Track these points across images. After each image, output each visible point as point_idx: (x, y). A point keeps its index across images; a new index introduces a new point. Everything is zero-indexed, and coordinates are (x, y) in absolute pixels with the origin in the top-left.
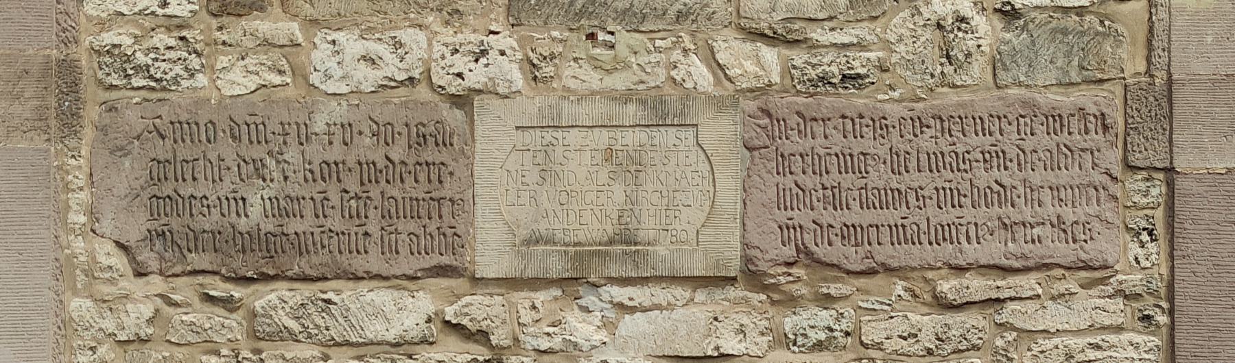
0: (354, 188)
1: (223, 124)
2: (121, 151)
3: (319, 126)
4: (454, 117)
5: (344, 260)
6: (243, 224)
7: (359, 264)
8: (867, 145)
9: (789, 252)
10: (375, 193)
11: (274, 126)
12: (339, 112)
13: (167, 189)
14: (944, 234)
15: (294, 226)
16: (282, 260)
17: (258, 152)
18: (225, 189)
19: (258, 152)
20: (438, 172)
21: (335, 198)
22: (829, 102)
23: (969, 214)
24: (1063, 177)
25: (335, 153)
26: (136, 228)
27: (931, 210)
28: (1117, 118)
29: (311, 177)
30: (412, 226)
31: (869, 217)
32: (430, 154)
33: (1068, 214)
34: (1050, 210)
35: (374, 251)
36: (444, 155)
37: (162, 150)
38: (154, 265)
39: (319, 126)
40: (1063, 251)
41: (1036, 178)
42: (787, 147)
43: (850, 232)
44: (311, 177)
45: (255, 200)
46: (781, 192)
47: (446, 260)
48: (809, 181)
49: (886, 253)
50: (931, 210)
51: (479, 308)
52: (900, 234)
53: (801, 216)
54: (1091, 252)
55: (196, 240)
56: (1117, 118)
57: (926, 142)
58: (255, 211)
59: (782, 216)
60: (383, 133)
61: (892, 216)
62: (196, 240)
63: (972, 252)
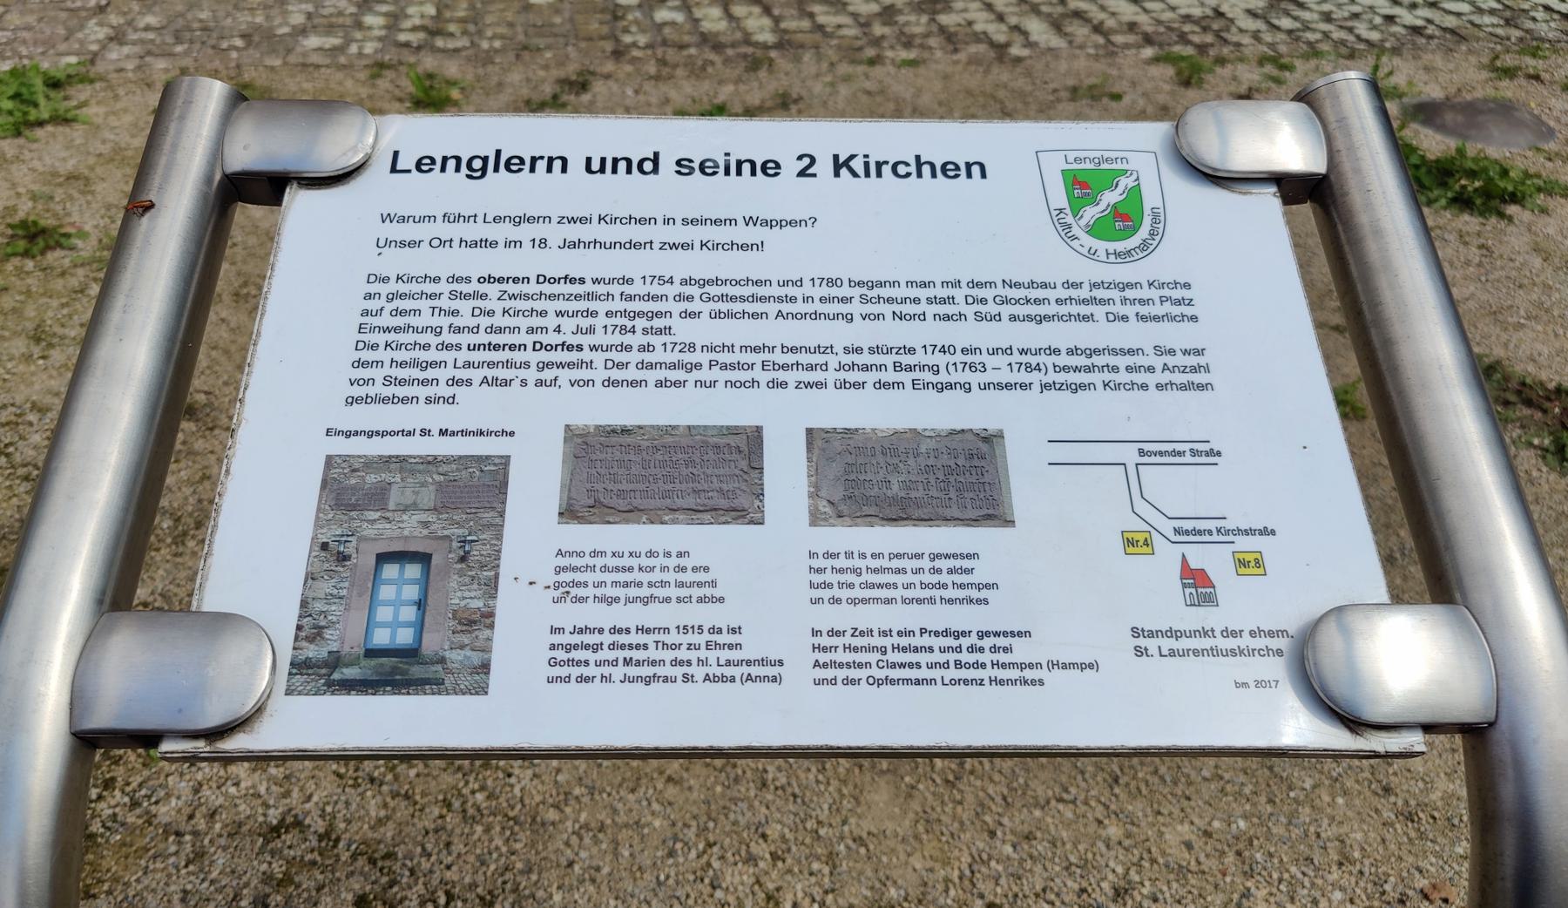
0: (942, 477)
1: (878, 449)
2: (830, 459)
3: (923, 450)
4: (984, 447)
5: (940, 511)
6: (889, 493)
7: (948, 513)
8: (632, 457)
9: (591, 502)
10: (952, 479)
11: (902, 449)
12: (932, 444)
13: (853, 477)
14: (666, 495)
15: (913, 494)
16: (909, 510)
17: (895, 461)
18: (880, 477)
19: (895, 461)
20: (981, 471)
21: (933, 482)
22: (614, 440)
23: (678, 486)
24: (722, 472)
25: (931, 462)
26: (837, 495)
27: (660, 483)
28: (744, 447)
29: (920, 472)
30: (971, 495)
31: (631, 486)
32: (976, 462)
33: (725, 487)
34: (716, 485)
35: (955, 507)
36: (983, 463)
37: (850, 459)
38: (846, 512)
39: (923, 450)
40: (723, 503)
41: (709, 472)
42: (594, 457)
43: (621, 494)
44: (920, 472)
45: (894, 481)
46: (589, 476)
47: (991, 512)
48: (603, 471)
49: (637, 502)
50: (660, 483)
51: (388, 514)
52: (646, 494)
53: (599, 487)
54: (736, 503)
55: (867, 500)
56: (744, 447)
57: (658, 456)
58: (895, 487)
59: (589, 486)
60: (952, 452)
61: (641, 487)
62: (867, 500)
63: (680, 503)
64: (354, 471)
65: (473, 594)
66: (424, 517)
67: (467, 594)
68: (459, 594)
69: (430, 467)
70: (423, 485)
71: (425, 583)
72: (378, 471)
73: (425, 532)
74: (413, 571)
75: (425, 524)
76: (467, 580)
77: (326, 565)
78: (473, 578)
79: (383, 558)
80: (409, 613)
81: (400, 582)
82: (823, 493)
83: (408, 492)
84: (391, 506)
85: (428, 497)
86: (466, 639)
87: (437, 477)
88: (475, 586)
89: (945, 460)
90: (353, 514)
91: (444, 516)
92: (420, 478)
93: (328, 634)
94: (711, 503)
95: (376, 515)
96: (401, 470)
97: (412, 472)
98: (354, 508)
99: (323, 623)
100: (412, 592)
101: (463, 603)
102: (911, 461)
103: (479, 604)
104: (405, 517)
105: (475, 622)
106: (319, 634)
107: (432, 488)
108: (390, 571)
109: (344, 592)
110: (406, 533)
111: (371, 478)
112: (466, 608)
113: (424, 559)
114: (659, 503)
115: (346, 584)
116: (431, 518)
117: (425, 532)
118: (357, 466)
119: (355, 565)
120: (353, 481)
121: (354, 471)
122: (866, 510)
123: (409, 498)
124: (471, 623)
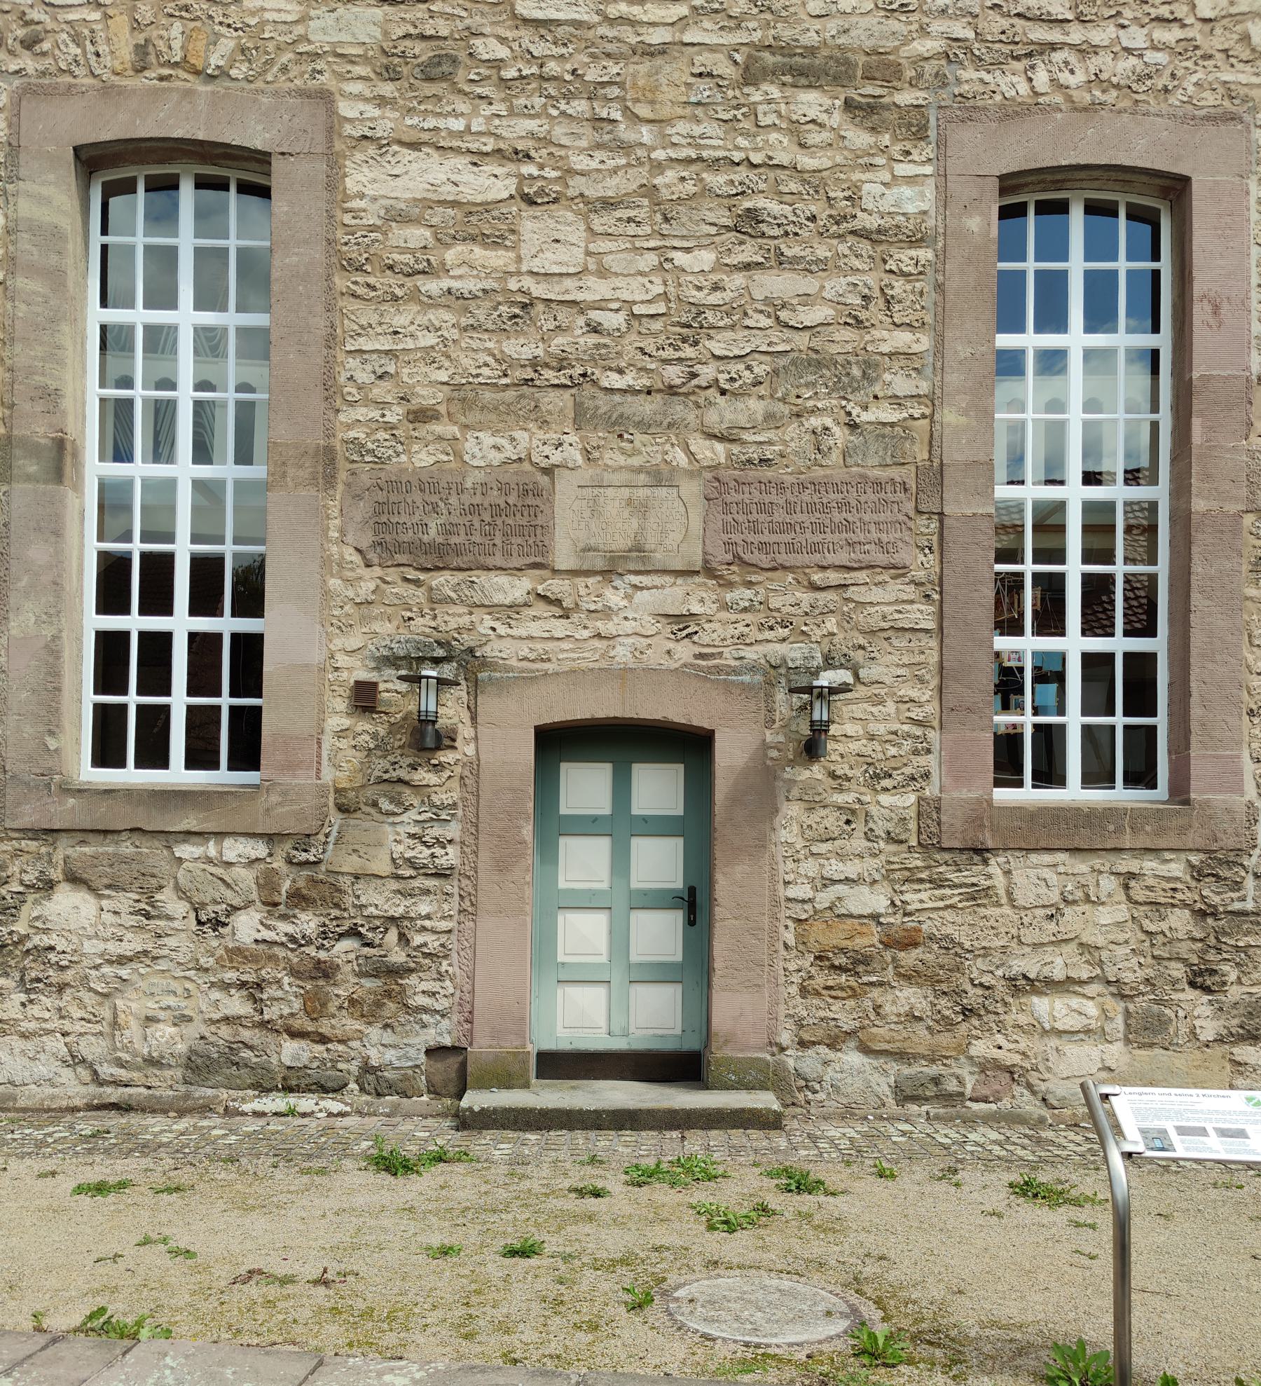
0: (488, 519)
1: (415, 483)
2: (359, 497)
3: (469, 485)
4: (544, 480)
5: (481, 559)
6: (425, 538)
7: (490, 561)
9: (729, 557)
10: (499, 522)
11: (443, 484)
12: (479, 476)
13: (384, 519)
15: (454, 540)
17: (434, 498)
18: (416, 519)
19: (434, 498)
20: (534, 511)
21: (477, 524)
25: (478, 499)
26: (366, 541)
29: (464, 513)
30: (519, 540)
32: (530, 501)
36: (538, 502)
37: (381, 497)
38: (376, 561)
39: (469, 485)
40: (882, 559)
44: (464, 513)
45: (432, 525)
47: (538, 560)
49: (783, 558)
51: (556, 586)
54: (897, 559)
58: (433, 531)
60: (504, 488)
62: (399, 547)
63: (830, 559)
64: (421, 416)
65: (851, 869)
66: (676, 596)
67: (835, 868)
68: (810, 867)
69: (679, 409)
70: (660, 477)
71: (697, 826)
72: (504, 417)
73: (685, 652)
74: (658, 787)
75: (682, 623)
76: (832, 821)
77: (380, 765)
78: (850, 815)
79: (558, 742)
80: (660, 935)
81: (621, 825)
82: (350, 538)
83: (613, 502)
84: (563, 557)
85: (680, 525)
86: (844, 1015)
87: (699, 445)
88: (859, 843)
89: (495, 497)
90: (443, 581)
91: (742, 595)
92: (649, 449)
93: (418, 987)
94: (866, 559)
95: (515, 588)
96: (581, 417)
97: (619, 426)
98: (438, 557)
99: (398, 956)
100: (658, 862)
101: (824, 898)
102: (453, 500)
103: (875, 900)
104: (614, 598)
105: (866, 960)
106: (398, 996)
107: (691, 489)
108: (585, 786)
109: (450, 857)
110: (622, 653)
111: (485, 449)
112: (836, 914)
113: (689, 746)
114: (805, 558)
115: (453, 830)
116: (696, 598)
117: (685, 652)
118: (427, 397)
119: (475, 766)
120: (423, 458)
121: (421, 416)
122: (400, 558)
123: (618, 532)
124: (858, 963)
